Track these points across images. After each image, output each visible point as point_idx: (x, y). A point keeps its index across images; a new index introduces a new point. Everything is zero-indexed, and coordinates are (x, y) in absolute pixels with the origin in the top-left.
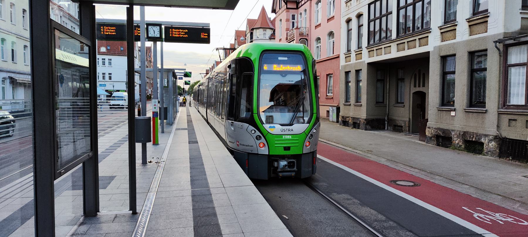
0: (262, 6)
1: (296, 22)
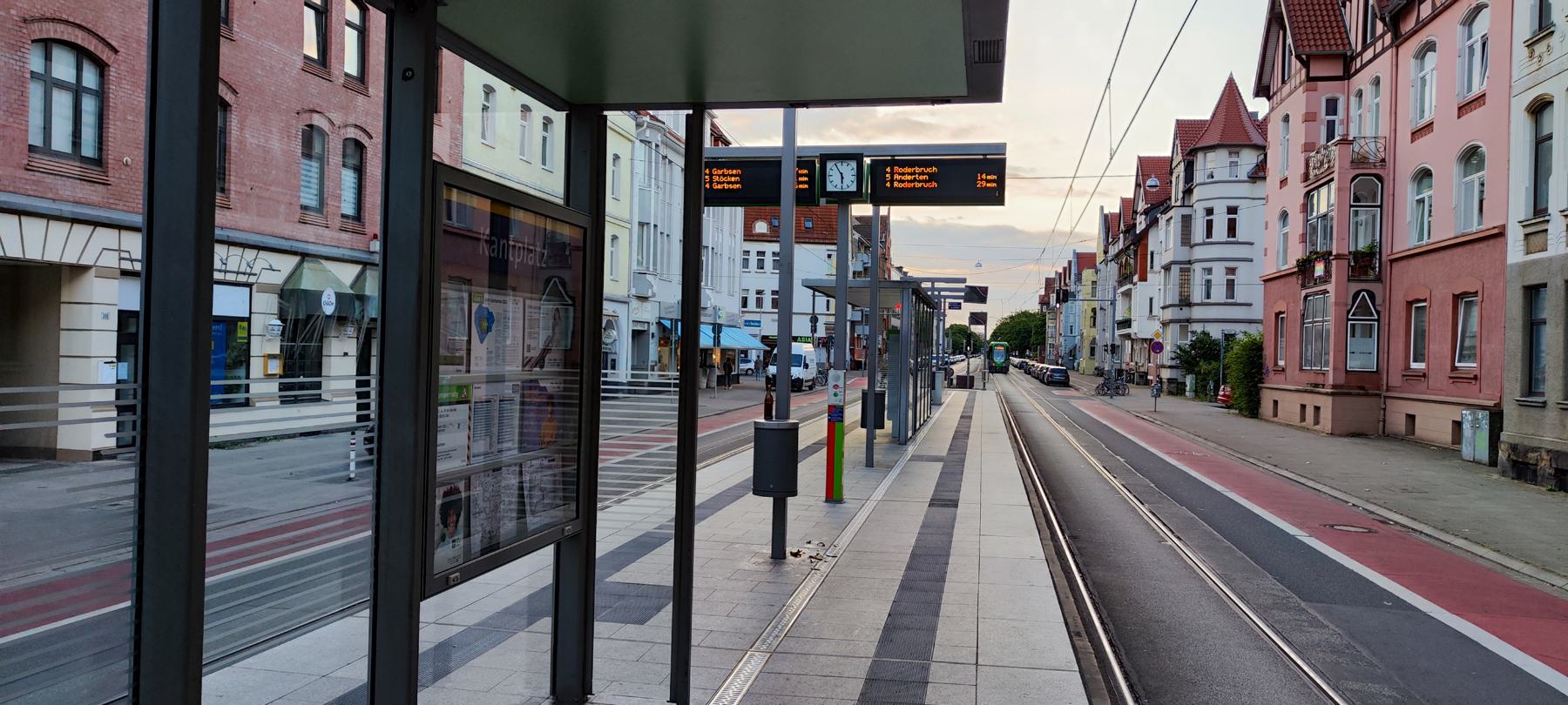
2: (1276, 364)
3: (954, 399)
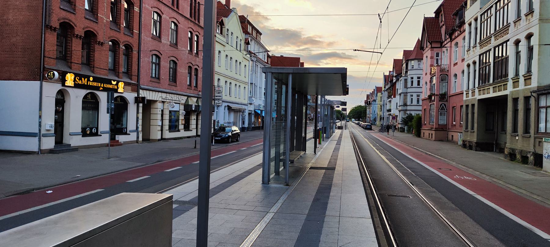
0: (418, 39)
1: (440, 59)
2: (424, 123)
3: (337, 132)
